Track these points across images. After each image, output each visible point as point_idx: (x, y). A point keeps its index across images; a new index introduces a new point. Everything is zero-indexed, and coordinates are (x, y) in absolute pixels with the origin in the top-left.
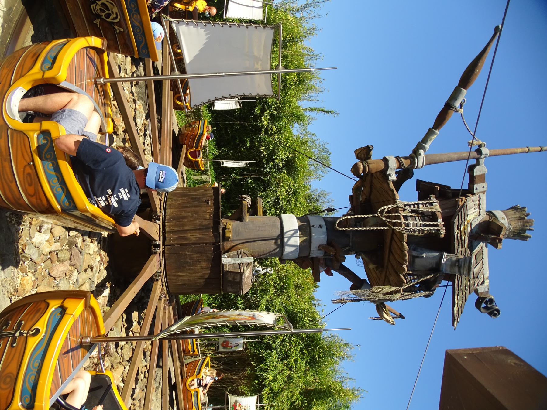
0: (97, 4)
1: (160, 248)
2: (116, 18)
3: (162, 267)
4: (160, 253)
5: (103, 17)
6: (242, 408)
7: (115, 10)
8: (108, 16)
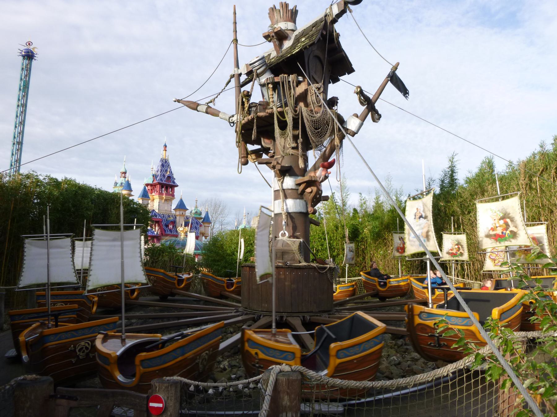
0: (79, 355)
1: (283, 316)
2: (88, 343)
3: (300, 315)
4: (310, 316)
5: (88, 351)
6: (454, 248)
7: (83, 343)
8: (87, 348)
